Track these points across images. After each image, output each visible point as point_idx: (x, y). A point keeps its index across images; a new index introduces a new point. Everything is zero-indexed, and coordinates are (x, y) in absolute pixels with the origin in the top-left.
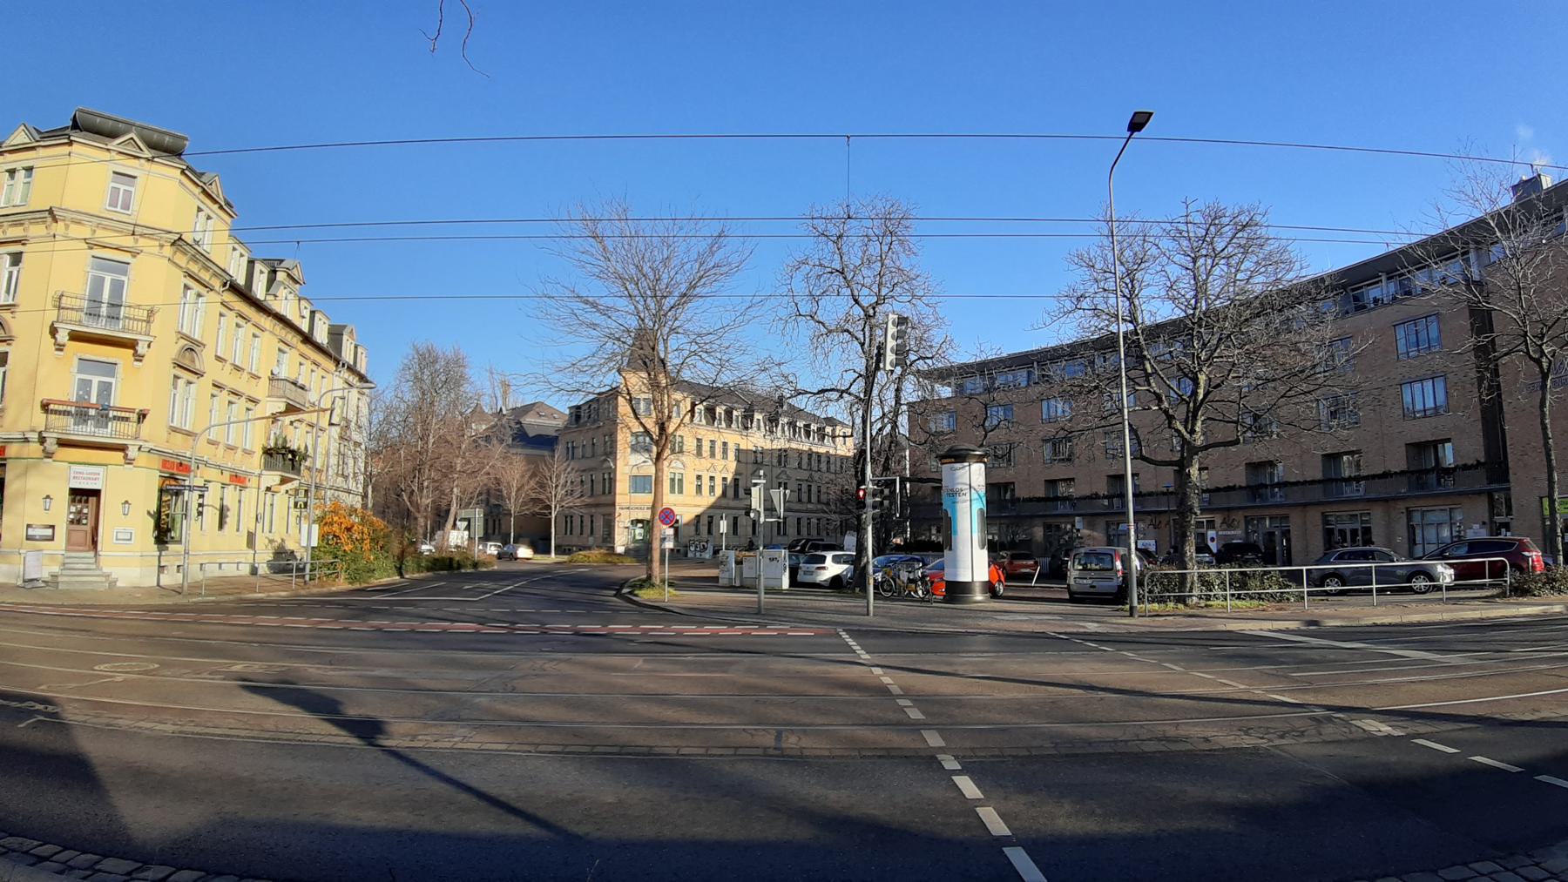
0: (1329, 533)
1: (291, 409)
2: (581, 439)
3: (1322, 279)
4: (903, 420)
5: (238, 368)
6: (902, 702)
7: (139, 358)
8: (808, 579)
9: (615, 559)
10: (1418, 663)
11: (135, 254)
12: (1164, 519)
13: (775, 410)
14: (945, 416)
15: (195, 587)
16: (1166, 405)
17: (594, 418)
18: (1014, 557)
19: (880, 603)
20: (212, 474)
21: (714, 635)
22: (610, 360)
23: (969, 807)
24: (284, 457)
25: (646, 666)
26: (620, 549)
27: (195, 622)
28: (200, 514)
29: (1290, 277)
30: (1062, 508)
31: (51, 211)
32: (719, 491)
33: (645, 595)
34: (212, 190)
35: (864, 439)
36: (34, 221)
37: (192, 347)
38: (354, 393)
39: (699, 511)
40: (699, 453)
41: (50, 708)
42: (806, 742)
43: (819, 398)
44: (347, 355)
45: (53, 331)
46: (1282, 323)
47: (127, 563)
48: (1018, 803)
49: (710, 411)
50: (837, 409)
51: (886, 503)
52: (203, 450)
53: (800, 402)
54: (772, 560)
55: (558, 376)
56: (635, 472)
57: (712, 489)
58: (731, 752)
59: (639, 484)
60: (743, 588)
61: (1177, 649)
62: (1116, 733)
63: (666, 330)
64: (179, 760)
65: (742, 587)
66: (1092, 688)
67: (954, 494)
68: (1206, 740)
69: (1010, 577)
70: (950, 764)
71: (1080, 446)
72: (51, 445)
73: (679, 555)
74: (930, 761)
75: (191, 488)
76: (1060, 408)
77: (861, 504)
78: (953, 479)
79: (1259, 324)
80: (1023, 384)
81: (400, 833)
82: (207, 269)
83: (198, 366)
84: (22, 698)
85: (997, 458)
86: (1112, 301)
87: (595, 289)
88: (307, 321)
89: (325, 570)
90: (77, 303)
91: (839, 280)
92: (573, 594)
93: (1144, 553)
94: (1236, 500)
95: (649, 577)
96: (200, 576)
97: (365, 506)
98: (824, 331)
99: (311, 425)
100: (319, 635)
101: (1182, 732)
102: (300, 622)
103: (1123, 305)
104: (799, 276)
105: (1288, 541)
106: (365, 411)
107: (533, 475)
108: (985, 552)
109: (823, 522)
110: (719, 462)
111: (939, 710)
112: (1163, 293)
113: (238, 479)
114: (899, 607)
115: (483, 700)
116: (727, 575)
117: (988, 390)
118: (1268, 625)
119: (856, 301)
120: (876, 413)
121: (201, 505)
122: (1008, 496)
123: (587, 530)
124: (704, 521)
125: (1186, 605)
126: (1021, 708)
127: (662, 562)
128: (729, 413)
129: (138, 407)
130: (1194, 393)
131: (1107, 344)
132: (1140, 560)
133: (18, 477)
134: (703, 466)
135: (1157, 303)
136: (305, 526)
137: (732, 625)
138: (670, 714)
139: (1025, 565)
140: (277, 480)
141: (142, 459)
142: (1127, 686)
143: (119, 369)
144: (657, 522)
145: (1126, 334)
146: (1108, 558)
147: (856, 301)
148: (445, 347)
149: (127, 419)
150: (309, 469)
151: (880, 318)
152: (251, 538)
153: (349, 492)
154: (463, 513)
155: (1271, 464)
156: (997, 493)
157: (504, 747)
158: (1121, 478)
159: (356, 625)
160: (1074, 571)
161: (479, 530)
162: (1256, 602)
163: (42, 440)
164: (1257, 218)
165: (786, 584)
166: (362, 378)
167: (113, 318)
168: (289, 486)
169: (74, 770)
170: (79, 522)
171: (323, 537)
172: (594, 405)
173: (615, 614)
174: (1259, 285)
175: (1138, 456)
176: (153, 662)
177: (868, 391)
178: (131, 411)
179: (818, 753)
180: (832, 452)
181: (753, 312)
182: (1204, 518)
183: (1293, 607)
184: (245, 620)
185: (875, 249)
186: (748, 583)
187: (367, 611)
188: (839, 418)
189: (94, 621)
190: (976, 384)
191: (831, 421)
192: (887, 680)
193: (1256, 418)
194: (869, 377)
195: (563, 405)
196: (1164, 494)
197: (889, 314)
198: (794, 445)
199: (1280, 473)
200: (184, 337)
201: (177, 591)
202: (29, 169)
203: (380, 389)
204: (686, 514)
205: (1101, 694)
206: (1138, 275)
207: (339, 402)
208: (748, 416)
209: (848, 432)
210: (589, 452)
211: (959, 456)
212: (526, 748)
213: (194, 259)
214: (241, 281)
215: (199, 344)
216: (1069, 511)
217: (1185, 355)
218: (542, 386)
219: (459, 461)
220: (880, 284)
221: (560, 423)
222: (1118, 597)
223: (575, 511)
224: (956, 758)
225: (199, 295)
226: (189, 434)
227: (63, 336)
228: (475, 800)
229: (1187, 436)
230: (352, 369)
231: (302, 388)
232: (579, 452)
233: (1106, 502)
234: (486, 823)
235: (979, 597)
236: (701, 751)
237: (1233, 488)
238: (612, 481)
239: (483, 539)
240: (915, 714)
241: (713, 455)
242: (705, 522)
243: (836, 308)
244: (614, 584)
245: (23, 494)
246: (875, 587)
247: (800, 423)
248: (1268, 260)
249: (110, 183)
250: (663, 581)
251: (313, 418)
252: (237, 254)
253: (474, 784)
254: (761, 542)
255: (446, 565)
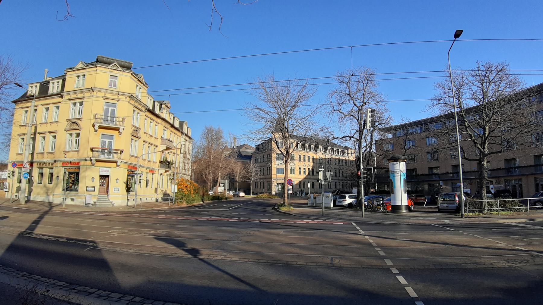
0: (537, 185)
1: (168, 148)
2: (260, 156)
3: (531, 89)
4: (374, 147)
5: (151, 136)
6: (376, 249)
7: (120, 133)
8: (340, 204)
9: (271, 197)
10: (499, 233)
11: (118, 101)
12: (474, 181)
13: (326, 144)
14: (389, 145)
15: (139, 205)
16: (474, 138)
17: (264, 149)
18: (417, 196)
19: (367, 213)
20: (144, 170)
21: (307, 223)
22: (269, 129)
23: (403, 286)
24: (166, 164)
25: (284, 233)
26: (273, 193)
27: (139, 217)
28: (140, 182)
29: (519, 89)
30: (434, 178)
31: (91, 88)
32: (307, 173)
33: (283, 209)
34: (141, 79)
35: (360, 154)
36: (87, 92)
37: (137, 130)
38: (187, 143)
39: (300, 180)
40: (300, 160)
41: (95, 244)
42: (342, 262)
43: (342, 140)
44: (185, 131)
45: (94, 126)
46: (517, 106)
47: (118, 198)
48: (420, 286)
49: (303, 146)
50: (349, 144)
51: (369, 177)
52: (141, 162)
53: (335, 141)
54: (327, 197)
55: (252, 135)
56: (278, 167)
57: (305, 172)
58: (315, 264)
59: (279, 171)
60: (317, 207)
61: (480, 230)
62: (458, 261)
63: (288, 118)
64: (136, 261)
65: (316, 206)
66: (448, 244)
67: (394, 173)
68: (492, 264)
69: (415, 204)
70: (395, 271)
71: (442, 155)
72: (94, 161)
73: (294, 195)
74: (387, 270)
75: (137, 174)
76: (433, 140)
77: (359, 177)
78: (393, 168)
79: (508, 107)
80: (419, 132)
81: (205, 287)
82: (140, 104)
83: (138, 136)
84: (86, 241)
85: (409, 160)
86: (452, 100)
87: (264, 105)
88: (172, 120)
89: (179, 200)
90: (101, 117)
91: (349, 97)
92: (258, 208)
93: (466, 194)
94: (501, 173)
95: (284, 203)
96: (140, 202)
97: (191, 179)
98: (343, 116)
99: (174, 153)
100: (178, 221)
101: (482, 261)
102: (172, 217)
103: (456, 102)
104: (334, 97)
105: (521, 189)
106: (191, 148)
107: (244, 169)
108: (406, 194)
109: (345, 184)
110: (307, 163)
111: (390, 252)
112: (470, 96)
113: (152, 171)
114: (374, 214)
115: (231, 243)
116: (311, 202)
117: (406, 135)
118: (514, 221)
119: (355, 105)
120: (364, 144)
121: (140, 180)
122: (414, 173)
123: (262, 187)
124: (302, 183)
125: (483, 213)
126: (421, 251)
127: (288, 198)
128: (310, 146)
129: (121, 149)
130: (484, 134)
131: (451, 116)
132: (465, 196)
133: (84, 171)
134: (301, 164)
135: (469, 100)
136: (173, 186)
137: (313, 220)
138: (293, 250)
139: (421, 199)
140: (164, 171)
141: (122, 165)
142: (461, 243)
143: (114, 137)
144: (286, 184)
145: (457, 112)
146: (453, 196)
147: (355, 105)
148: (215, 127)
149: (117, 153)
150: (174, 167)
151: (364, 110)
152: (156, 190)
153: (186, 175)
154: (222, 181)
155: (515, 159)
156: (411, 174)
157: (238, 259)
158: (458, 166)
159: (190, 218)
160: (440, 201)
161: (227, 188)
162: (509, 212)
163: (91, 160)
164: (505, 67)
165: (332, 206)
166: (190, 138)
167: (112, 121)
168: (168, 173)
169: (103, 264)
170: (103, 185)
171: (179, 189)
172: (264, 145)
173: (273, 216)
174: (507, 92)
175: (464, 158)
176: (126, 230)
177: (361, 136)
178: (119, 150)
179: (346, 266)
180: (347, 159)
181: (318, 110)
182: (489, 180)
183: (524, 214)
184: (155, 216)
185: (361, 86)
186: (318, 205)
187: (192, 214)
188: (350, 147)
189: (108, 216)
190: (401, 133)
191: (346, 148)
192: (371, 241)
193: (508, 142)
194: (361, 132)
195: (253, 145)
196: (473, 172)
197: (368, 109)
198: (334, 157)
199: (518, 163)
200: (134, 126)
201: (133, 207)
202: (84, 75)
203: (196, 141)
204: (296, 181)
205: (451, 246)
206: (461, 90)
207: (183, 146)
208: (317, 147)
209: (353, 151)
210: (262, 160)
211: (396, 159)
212: (245, 260)
213: (136, 102)
214: (151, 108)
215: (139, 128)
216: (437, 179)
217: (480, 119)
218: (247, 139)
219: (221, 164)
220: (364, 98)
221: (253, 151)
222: (457, 210)
223: (259, 181)
224: (397, 269)
225: (138, 113)
226: (136, 157)
227: (97, 127)
228: (229, 277)
229: (482, 150)
230: (186, 135)
231: (171, 141)
232: (259, 160)
233: (451, 175)
234: (233, 285)
235: (404, 211)
236: (305, 264)
237: (500, 169)
238: (270, 170)
239: (231, 190)
240: (382, 253)
241: (304, 160)
242: (302, 184)
243: (347, 108)
244: (272, 205)
245: (85, 177)
246: (365, 207)
247: (335, 148)
248: (511, 83)
249: (109, 79)
250: (289, 204)
251: (175, 151)
252: (149, 99)
253: (229, 272)
254: (323, 191)
255: (217, 198)
